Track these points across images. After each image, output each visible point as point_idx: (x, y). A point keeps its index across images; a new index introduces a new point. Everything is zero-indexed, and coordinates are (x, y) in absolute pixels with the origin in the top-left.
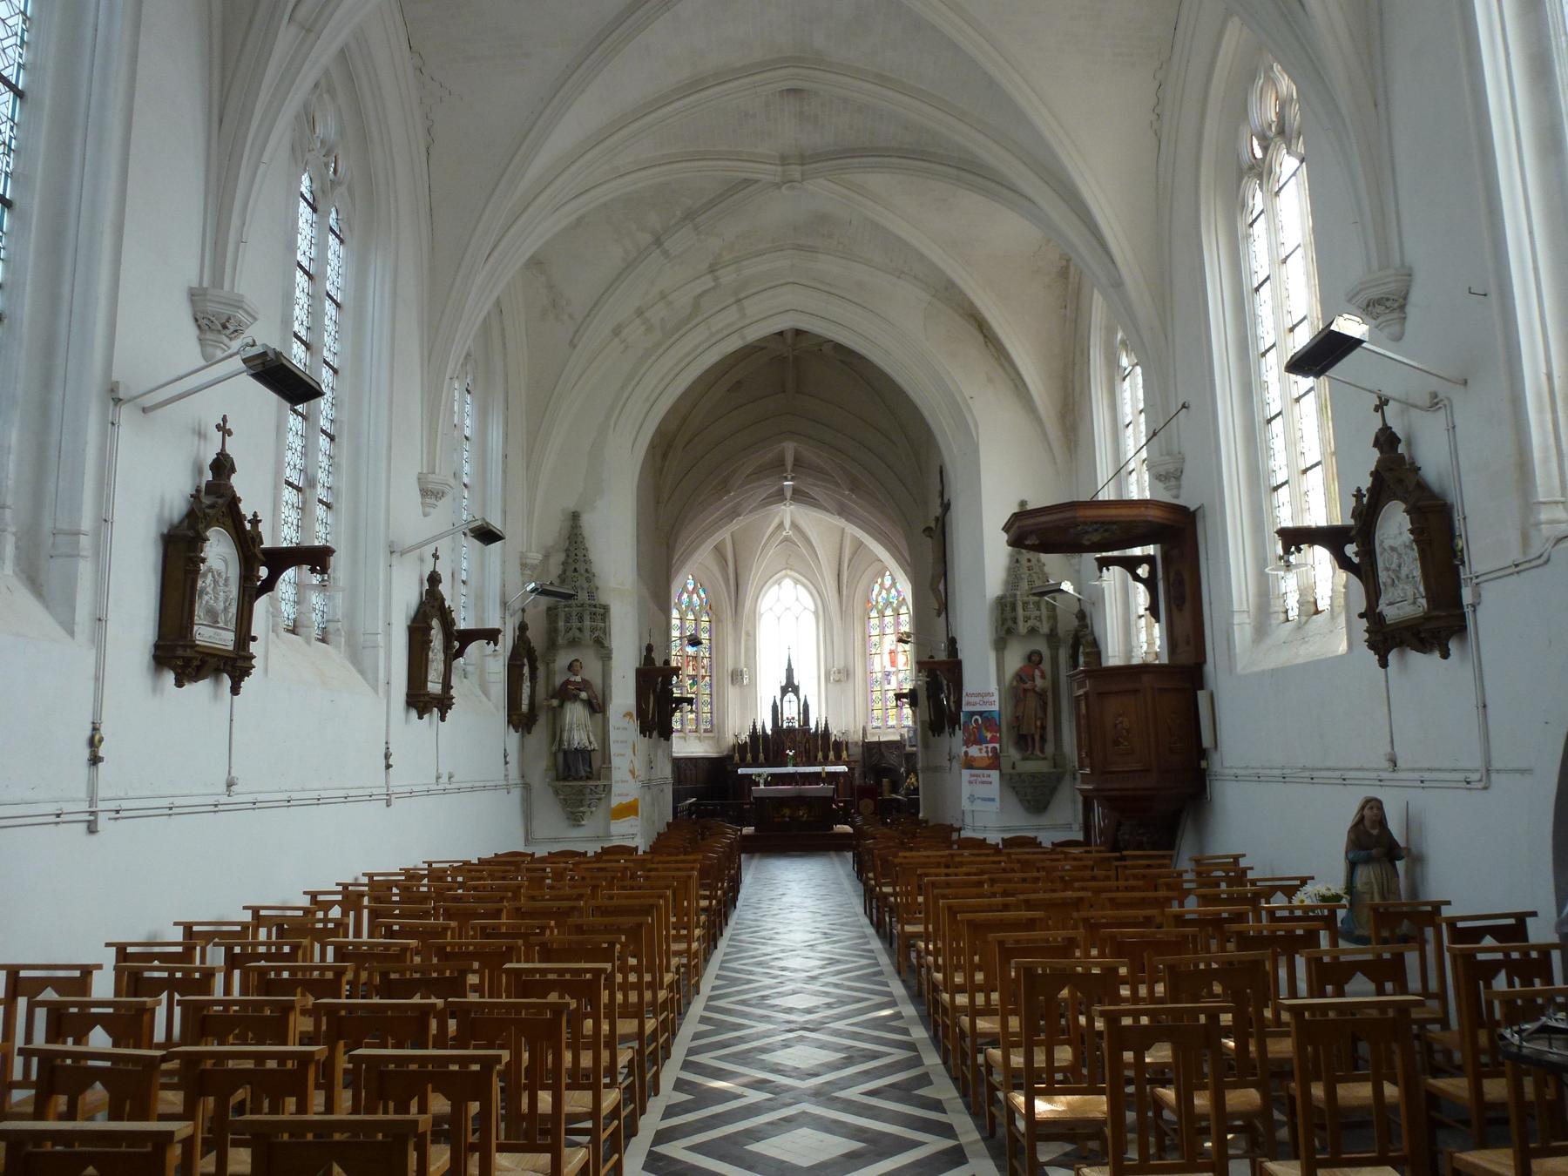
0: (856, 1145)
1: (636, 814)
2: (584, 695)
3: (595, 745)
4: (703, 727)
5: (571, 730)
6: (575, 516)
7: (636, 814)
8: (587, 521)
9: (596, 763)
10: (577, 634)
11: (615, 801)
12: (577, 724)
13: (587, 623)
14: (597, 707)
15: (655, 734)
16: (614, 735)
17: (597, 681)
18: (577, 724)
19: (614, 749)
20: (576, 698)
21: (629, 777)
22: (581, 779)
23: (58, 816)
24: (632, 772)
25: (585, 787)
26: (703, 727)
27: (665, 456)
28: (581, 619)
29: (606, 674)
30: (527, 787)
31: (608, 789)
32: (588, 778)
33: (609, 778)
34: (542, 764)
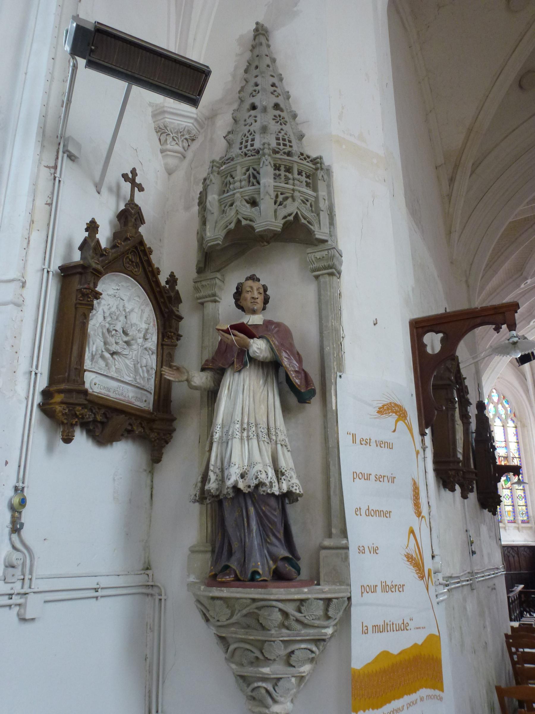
0: (136, 189)
1: (435, 680)
2: (258, 347)
3: (292, 482)
4: (520, 518)
5: (225, 442)
6: (261, 33)
7: (435, 680)
8: (281, 41)
9: (307, 533)
10: (247, 210)
11: (364, 650)
12: (247, 434)
13: (267, 180)
14: (302, 388)
15: (473, 496)
16: (352, 459)
17: (303, 325)
18: (247, 434)
19: (355, 495)
20: (243, 359)
21: (408, 574)
22: (254, 578)
23: (96, 590)
24: (416, 562)
25: (264, 605)
26: (520, 518)
27: (452, 180)
28: (254, 178)
29: (327, 310)
30: (148, 589)
31: (339, 610)
32: (279, 576)
33: (342, 578)
34: (186, 533)
